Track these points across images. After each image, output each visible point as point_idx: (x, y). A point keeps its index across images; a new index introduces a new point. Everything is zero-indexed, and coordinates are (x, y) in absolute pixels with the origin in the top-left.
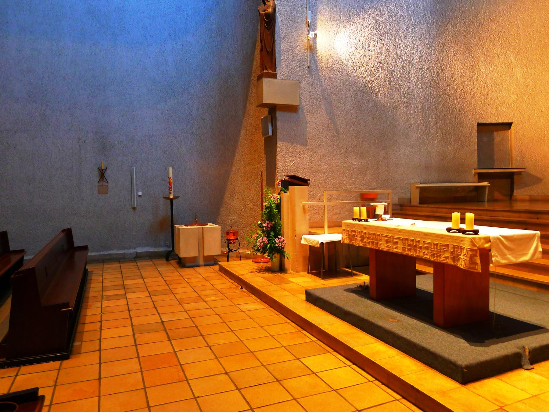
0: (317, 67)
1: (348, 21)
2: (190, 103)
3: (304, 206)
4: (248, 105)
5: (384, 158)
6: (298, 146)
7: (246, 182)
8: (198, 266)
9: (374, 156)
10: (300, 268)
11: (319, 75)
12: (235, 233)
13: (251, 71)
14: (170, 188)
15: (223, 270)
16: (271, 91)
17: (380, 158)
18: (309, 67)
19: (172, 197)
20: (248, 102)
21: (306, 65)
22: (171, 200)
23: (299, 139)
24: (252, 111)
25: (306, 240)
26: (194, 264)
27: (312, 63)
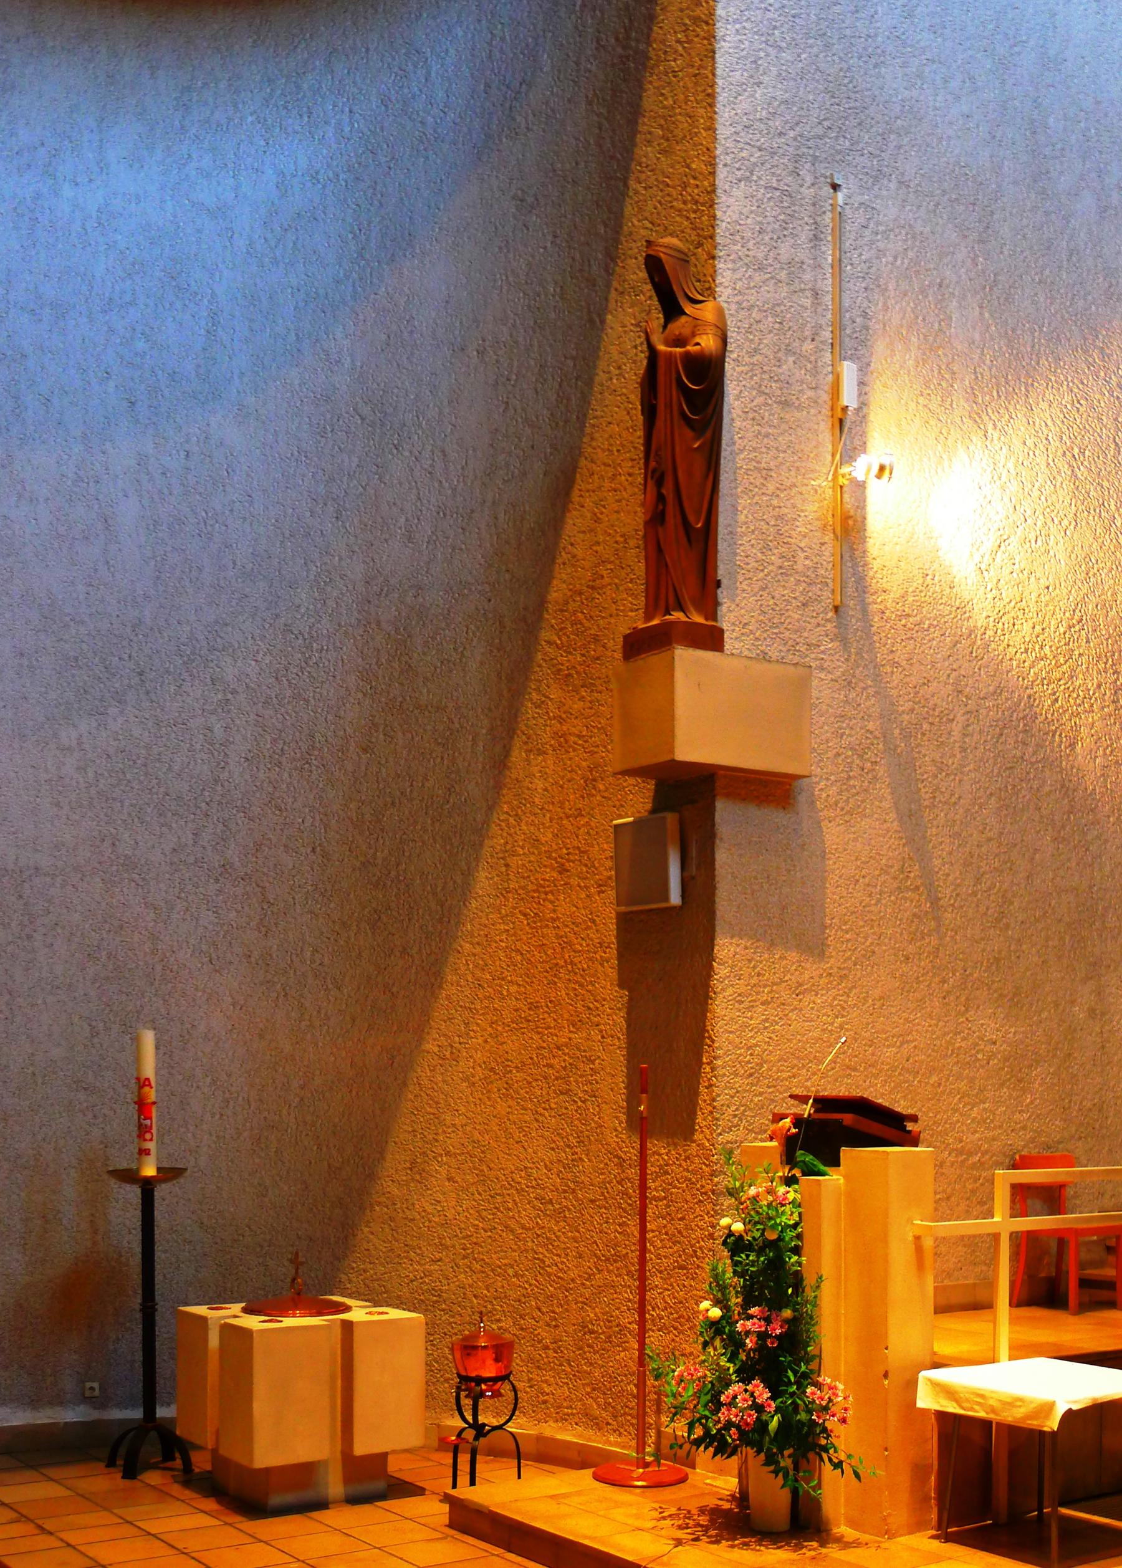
0: (865, 611)
1: (976, 418)
2: (218, 729)
3: (917, 1238)
4: (517, 756)
5: (1092, 1012)
6: (793, 955)
7: (502, 1107)
8: (321, 1505)
9: (1057, 1005)
10: (900, 1516)
11: (871, 650)
12: (502, 1350)
13: (542, 603)
14: (143, 1131)
15: (471, 1521)
16: (707, 712)
17: (1079, 1013)
18: (836, 609)
19: (150, 1171)
20: (517, 743)
21: (827, 599)
22: (148, 1187)
23: (797, 929)
24: (540, 784)
25: (936, 1385)
26: (308, 1495)
27: (850, 591)
